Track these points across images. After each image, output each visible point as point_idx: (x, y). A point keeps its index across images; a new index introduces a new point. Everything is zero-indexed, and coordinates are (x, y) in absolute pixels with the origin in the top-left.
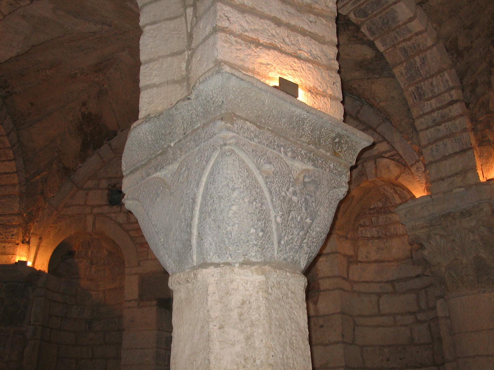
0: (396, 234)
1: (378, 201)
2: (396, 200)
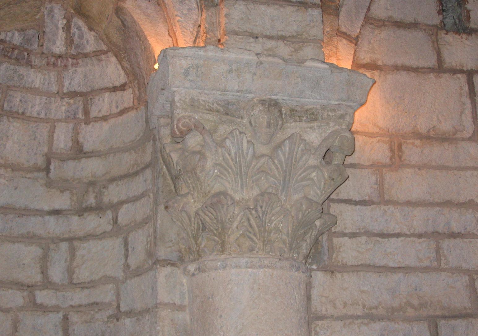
0: (23, 113)
1: (18, 31)
2: (54, 44)
